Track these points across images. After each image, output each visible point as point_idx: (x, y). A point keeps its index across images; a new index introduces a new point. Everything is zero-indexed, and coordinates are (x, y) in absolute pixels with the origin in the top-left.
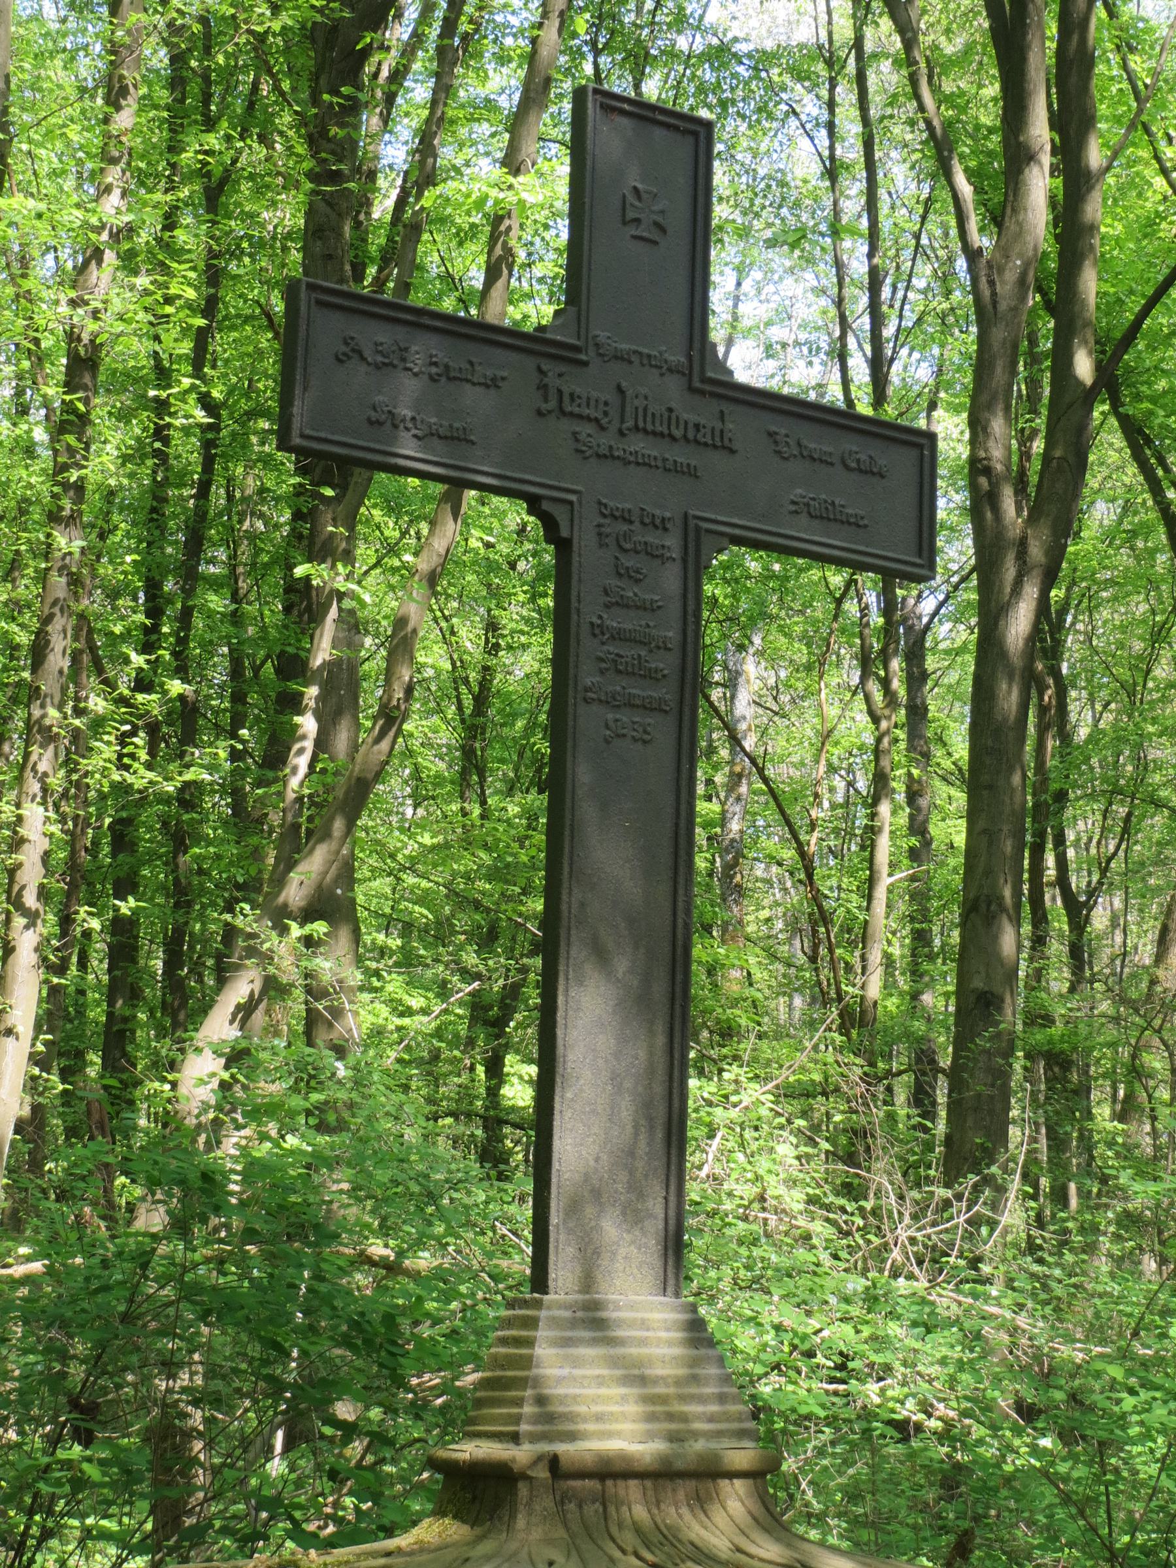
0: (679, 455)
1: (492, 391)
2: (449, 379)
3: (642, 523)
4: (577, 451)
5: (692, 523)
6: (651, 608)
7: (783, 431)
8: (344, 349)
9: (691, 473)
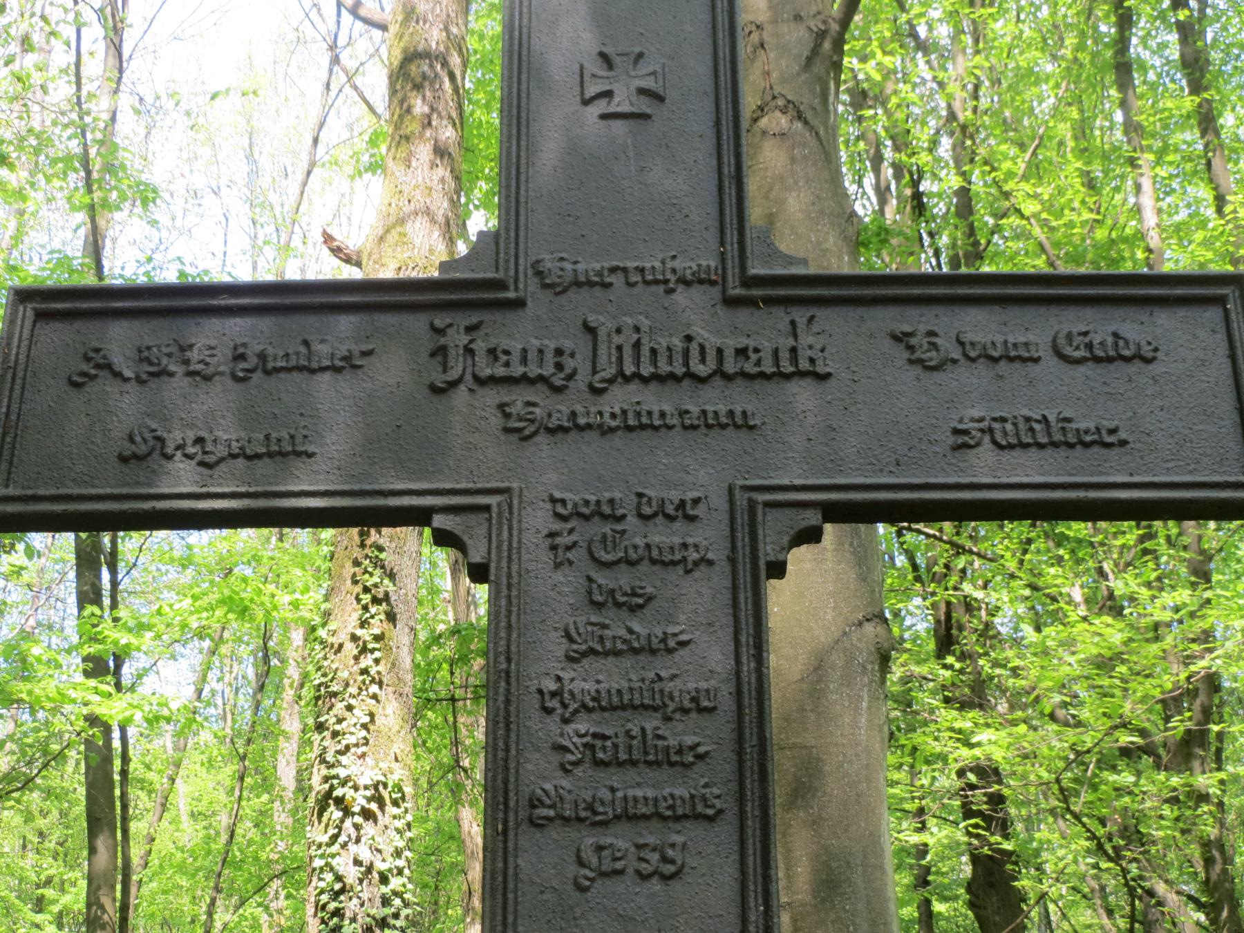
0: (715, 399)
1: (347, 375)
2: (268, 373)
3: (641, 516)
4: (507, 430)
5: (741, 499)
6: (665, 647)
7: (922, 328)
8: (85, 367)
9: (743, 424)
